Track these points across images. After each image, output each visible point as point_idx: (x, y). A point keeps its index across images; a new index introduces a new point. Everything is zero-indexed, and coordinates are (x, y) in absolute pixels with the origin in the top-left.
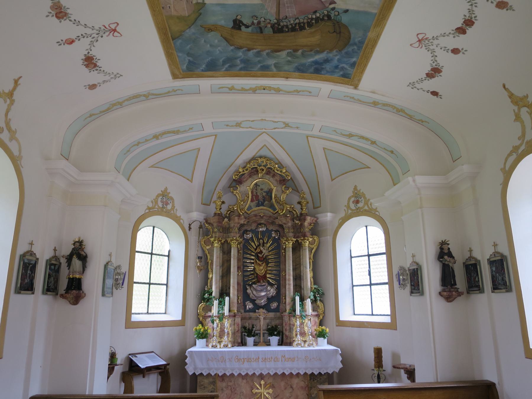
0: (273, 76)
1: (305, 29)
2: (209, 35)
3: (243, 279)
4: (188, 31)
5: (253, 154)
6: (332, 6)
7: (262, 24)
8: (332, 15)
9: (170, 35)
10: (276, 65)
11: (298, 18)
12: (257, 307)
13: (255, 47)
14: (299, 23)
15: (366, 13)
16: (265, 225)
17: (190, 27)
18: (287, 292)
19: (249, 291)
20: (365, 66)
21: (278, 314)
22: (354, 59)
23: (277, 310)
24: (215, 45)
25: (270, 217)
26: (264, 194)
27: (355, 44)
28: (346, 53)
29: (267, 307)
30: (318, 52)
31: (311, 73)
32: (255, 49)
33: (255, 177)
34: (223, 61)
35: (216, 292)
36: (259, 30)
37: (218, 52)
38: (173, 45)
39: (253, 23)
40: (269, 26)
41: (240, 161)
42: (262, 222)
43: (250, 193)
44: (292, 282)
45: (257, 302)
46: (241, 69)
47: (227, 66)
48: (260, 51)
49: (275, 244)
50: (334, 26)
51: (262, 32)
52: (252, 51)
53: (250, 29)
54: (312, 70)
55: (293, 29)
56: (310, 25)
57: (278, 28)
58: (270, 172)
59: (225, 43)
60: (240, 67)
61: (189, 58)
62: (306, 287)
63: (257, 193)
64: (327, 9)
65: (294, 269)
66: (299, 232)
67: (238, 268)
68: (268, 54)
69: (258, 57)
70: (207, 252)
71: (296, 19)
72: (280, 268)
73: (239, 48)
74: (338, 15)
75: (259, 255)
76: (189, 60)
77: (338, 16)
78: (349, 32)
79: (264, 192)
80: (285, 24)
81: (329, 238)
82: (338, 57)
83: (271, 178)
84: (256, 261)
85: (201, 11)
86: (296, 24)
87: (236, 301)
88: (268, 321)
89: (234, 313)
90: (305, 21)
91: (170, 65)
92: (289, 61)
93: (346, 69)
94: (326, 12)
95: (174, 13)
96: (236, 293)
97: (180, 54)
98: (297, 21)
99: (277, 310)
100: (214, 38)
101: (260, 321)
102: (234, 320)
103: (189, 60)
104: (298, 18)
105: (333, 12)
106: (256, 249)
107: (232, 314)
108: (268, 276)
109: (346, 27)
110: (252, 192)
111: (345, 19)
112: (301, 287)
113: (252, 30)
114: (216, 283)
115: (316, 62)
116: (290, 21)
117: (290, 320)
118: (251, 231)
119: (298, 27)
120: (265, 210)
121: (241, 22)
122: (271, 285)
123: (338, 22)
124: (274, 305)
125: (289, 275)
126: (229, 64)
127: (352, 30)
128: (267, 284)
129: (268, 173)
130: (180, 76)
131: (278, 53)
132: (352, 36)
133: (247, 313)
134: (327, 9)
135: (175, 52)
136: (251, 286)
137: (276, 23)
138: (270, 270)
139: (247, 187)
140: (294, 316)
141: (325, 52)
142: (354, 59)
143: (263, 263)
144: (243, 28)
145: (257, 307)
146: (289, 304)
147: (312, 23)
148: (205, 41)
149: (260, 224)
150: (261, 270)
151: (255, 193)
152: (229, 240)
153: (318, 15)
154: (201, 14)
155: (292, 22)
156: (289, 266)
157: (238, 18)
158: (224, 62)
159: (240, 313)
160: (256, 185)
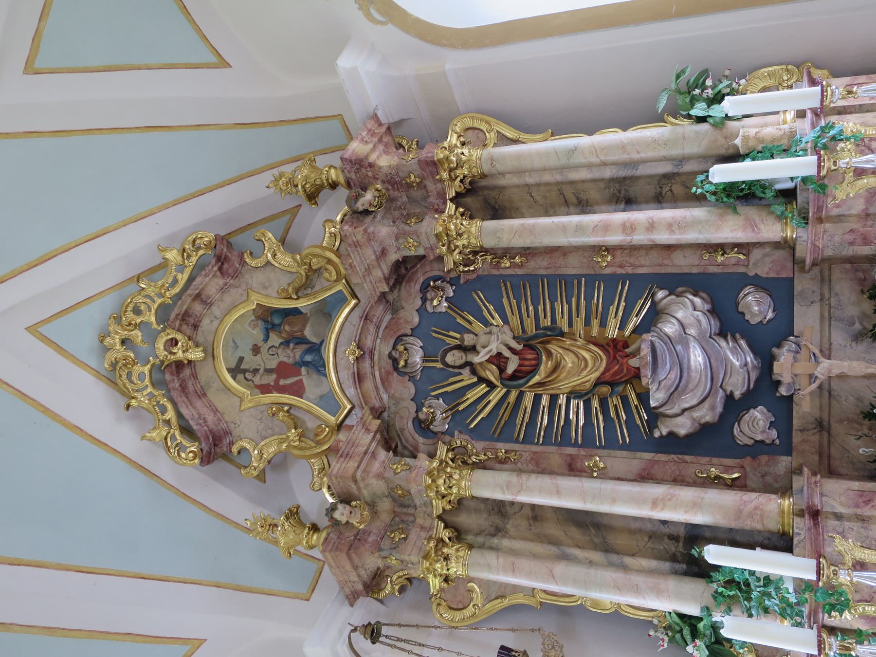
3: (624, 447)
5: (89, 380)
12: (765, 388)
16: (399, 340)
18: (692, 236)
19: (683, 426)
21: (801, 284)
23: (781, 293)
25: (366, 318)
26: (275, 339)
29: (765, 343)
33: (205, 373)
35: (680, 596)
41: (125, 436)
42: (386, 349)
43: (276, 397)
44: (640, 216)
45: (738, 386)
49: (479, 297)
58: (182, 317)
62: (666, 143)
63: (268, 371)
65: (584, 206)
66: (405, 196)
67: (573, 469)
70: (498, 604)
72: (579, 277)
75: (511, 369)
79: (266, 339)
81: (454, 62)
83: (216, 310)
84: (540, 384)
87: (729, 498)
88: (839, 338)
89: (800, 514)
96: (687, 493)
99: (781, 293)
101: (842, 377)
102: (838, 517)
106: (492, 386)
107: (800, 528)
108: (612, 332)
110: (265, 389)
112: (668, 177)
114: (636, 590)
117: (840, 219)
118: (418, 400)
120: (339, 337)
122: (655, 315)
124: (756, 306)
125: (606, 228)
128: (647, 337)
129: (189, 322)
133: (796, 438)
136: (655, 416)
138: (588, 323)
139: (240, 406)
140: (819, 184)
143: (549, 354)
145: (765, 388)
146: (753, 226)
149: (395, 361)
150: (577, 365)
151: (270, 379)
152: (439, 505)
156: (564, 228)
159: (798, 482)
160: (235, 372)
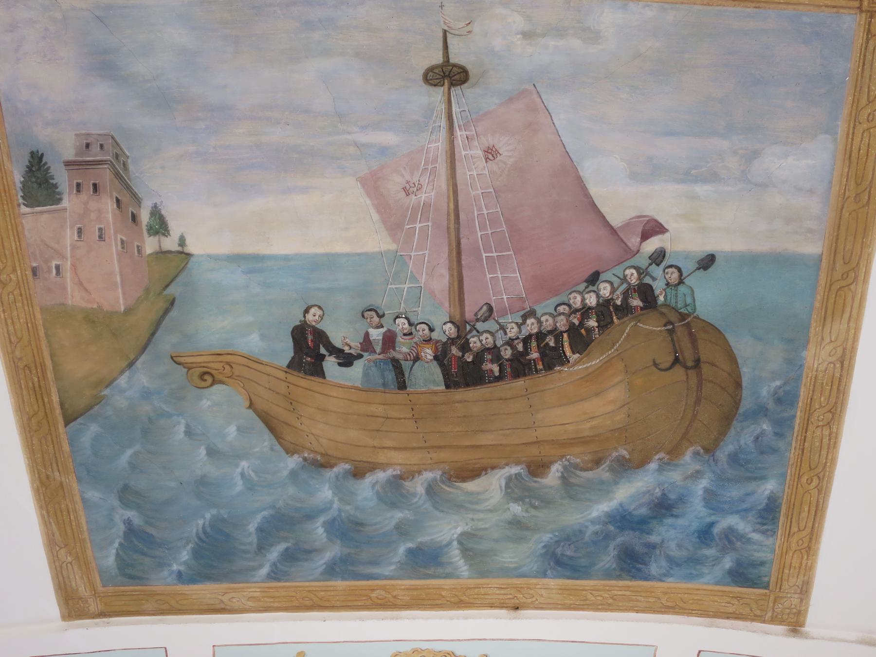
0: (460, 603)
1: (563, 360)
2: (205, 403)
4: (123, 381)
6: (652, 245)
7: (403, 348)
8: (658, 287)
9: (55, 399)
10: (469, 544)
11: (532, 313)
13: (382, 457)
14: (540, 336)
15: (782, 261)
17: (131, 364)
20: (818, 511)
22: (769, 487)
24: (221, 450)
27: (761, 411)
28: (734, 459)
30: (626, 467)
31: (608, 575)
32: (383, 467)
34: (260, 530)
36: (390, 376)
37: (239, 486)
38: (66, 447)
39: (367, 344)
40: (428, 353)
46: (331, 571)
47: (274, 554)
48: (401, 477)
50: (671, 332)
51: (402, 385)
52: (369, 479)
53: (358, 369)
54: (608, 559)
55: (520, 367)
56: (581, 340)
57: (463, 365)
59: (264, 441)
60: (328, 555)
61: (131, 514)
64: (634, 261)
68: (431, 490)
69: (394, 505)
71: (525, 317)
73: (322, 464)
74: (681, 282)
76: (128, 523)
77: (682, 289)
78: (732, 358)
80: (487, 340)
82: (704, 483)
85: (172, 290)
86: (526, 341)
90: (562, 323)
91: (51, 544)
92: (516, 523)
93: (742, 537)
94: (633, 276)
95: (74, 298)
97: (93, 495)
98: (531, 327)
100: (222, 412)
103: (128, 523)
104: (532, 313)
105: (657, 271)
109: (709, 327)
111: (707, 298)
113: (366, 374)
115: (622, 520)
116: (503, 328)
119: (535, 355)
121: (321, 336)
123: (683, 317)
126: (282, 547)
127: (743, 346)
130: (94, 606)
131: (470, 486)
132: (746, 372)
134: (634, 261)
135: (75, 486)
137: (452, 341)
141: (653, 466)
142: (769, 487)
144: (330, 364)
147: (589, 330)
148: (188, 433)
153: (605, 290)
154: (172, 303)
155: (513, 331)
157: (310, 317)
158: (266, 536)
